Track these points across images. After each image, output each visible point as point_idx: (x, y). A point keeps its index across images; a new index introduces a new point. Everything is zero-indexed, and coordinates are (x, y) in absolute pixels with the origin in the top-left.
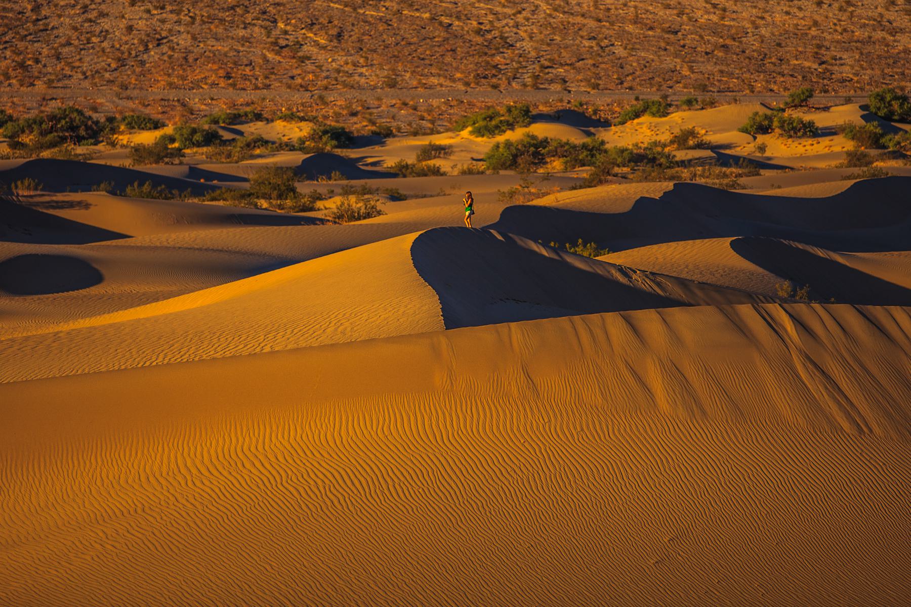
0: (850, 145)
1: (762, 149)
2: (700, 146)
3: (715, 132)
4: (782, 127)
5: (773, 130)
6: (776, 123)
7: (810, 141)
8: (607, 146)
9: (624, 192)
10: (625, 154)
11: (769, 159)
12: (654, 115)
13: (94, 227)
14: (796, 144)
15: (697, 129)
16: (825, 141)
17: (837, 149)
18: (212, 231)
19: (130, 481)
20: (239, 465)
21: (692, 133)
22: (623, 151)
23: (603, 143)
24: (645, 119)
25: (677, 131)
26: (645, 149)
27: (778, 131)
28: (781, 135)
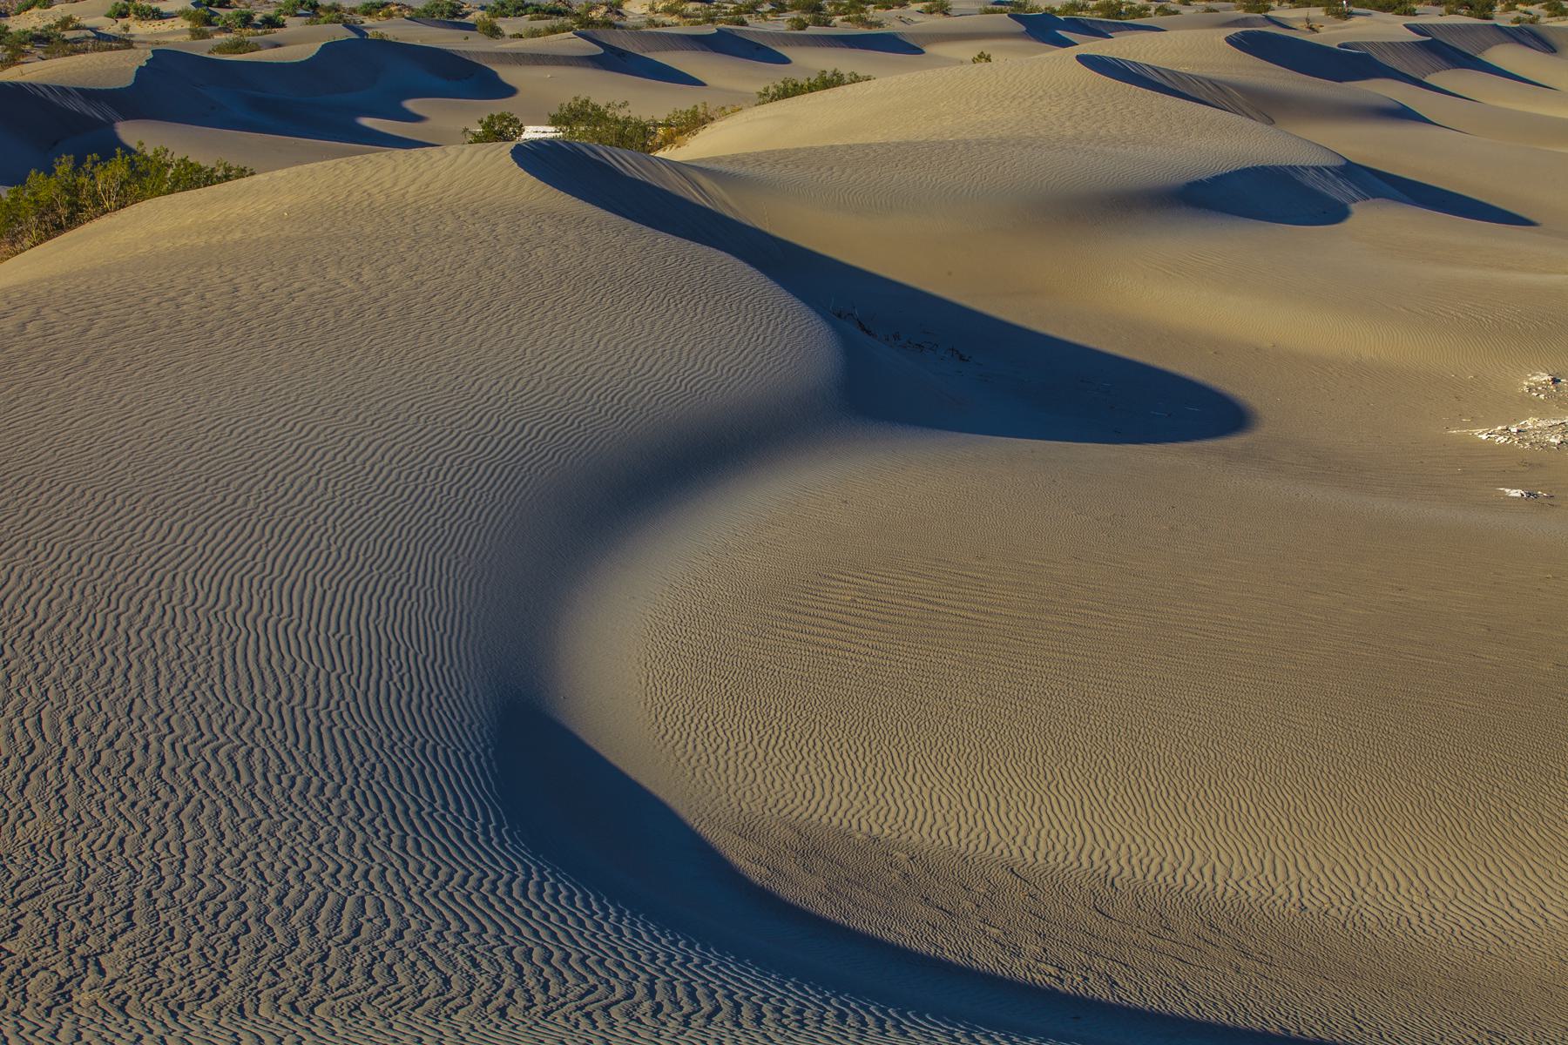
0: (187, 25)
1: (126, 28)
2: (78, 28)
3: (86, 18)
4: (136, 13)
5: (129, 15)
6: (132, 10)
7: (158, 22)
8: (10, 30)
9: (98, 62)
10: (27, 35)
11: (132, 36)
12: (41, 7)
13: (1425, 185)
14: (147, 25)
15: (74, 17)
16: (169, 22)
17: (178, 27)
18: (904, 77)
19: (106, 650)
20: (967, 742)
21: (70, 19)
22: (25, 33)
23: (7, 28)
24: (35, 10)
25: (58, 19)
26: (42, 30)
27: (133, 15)
28: (136, 19)
